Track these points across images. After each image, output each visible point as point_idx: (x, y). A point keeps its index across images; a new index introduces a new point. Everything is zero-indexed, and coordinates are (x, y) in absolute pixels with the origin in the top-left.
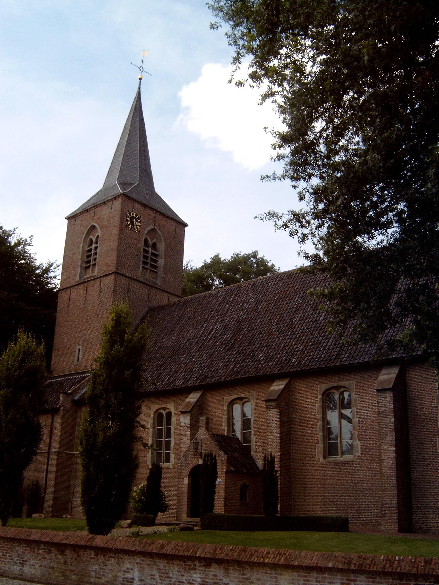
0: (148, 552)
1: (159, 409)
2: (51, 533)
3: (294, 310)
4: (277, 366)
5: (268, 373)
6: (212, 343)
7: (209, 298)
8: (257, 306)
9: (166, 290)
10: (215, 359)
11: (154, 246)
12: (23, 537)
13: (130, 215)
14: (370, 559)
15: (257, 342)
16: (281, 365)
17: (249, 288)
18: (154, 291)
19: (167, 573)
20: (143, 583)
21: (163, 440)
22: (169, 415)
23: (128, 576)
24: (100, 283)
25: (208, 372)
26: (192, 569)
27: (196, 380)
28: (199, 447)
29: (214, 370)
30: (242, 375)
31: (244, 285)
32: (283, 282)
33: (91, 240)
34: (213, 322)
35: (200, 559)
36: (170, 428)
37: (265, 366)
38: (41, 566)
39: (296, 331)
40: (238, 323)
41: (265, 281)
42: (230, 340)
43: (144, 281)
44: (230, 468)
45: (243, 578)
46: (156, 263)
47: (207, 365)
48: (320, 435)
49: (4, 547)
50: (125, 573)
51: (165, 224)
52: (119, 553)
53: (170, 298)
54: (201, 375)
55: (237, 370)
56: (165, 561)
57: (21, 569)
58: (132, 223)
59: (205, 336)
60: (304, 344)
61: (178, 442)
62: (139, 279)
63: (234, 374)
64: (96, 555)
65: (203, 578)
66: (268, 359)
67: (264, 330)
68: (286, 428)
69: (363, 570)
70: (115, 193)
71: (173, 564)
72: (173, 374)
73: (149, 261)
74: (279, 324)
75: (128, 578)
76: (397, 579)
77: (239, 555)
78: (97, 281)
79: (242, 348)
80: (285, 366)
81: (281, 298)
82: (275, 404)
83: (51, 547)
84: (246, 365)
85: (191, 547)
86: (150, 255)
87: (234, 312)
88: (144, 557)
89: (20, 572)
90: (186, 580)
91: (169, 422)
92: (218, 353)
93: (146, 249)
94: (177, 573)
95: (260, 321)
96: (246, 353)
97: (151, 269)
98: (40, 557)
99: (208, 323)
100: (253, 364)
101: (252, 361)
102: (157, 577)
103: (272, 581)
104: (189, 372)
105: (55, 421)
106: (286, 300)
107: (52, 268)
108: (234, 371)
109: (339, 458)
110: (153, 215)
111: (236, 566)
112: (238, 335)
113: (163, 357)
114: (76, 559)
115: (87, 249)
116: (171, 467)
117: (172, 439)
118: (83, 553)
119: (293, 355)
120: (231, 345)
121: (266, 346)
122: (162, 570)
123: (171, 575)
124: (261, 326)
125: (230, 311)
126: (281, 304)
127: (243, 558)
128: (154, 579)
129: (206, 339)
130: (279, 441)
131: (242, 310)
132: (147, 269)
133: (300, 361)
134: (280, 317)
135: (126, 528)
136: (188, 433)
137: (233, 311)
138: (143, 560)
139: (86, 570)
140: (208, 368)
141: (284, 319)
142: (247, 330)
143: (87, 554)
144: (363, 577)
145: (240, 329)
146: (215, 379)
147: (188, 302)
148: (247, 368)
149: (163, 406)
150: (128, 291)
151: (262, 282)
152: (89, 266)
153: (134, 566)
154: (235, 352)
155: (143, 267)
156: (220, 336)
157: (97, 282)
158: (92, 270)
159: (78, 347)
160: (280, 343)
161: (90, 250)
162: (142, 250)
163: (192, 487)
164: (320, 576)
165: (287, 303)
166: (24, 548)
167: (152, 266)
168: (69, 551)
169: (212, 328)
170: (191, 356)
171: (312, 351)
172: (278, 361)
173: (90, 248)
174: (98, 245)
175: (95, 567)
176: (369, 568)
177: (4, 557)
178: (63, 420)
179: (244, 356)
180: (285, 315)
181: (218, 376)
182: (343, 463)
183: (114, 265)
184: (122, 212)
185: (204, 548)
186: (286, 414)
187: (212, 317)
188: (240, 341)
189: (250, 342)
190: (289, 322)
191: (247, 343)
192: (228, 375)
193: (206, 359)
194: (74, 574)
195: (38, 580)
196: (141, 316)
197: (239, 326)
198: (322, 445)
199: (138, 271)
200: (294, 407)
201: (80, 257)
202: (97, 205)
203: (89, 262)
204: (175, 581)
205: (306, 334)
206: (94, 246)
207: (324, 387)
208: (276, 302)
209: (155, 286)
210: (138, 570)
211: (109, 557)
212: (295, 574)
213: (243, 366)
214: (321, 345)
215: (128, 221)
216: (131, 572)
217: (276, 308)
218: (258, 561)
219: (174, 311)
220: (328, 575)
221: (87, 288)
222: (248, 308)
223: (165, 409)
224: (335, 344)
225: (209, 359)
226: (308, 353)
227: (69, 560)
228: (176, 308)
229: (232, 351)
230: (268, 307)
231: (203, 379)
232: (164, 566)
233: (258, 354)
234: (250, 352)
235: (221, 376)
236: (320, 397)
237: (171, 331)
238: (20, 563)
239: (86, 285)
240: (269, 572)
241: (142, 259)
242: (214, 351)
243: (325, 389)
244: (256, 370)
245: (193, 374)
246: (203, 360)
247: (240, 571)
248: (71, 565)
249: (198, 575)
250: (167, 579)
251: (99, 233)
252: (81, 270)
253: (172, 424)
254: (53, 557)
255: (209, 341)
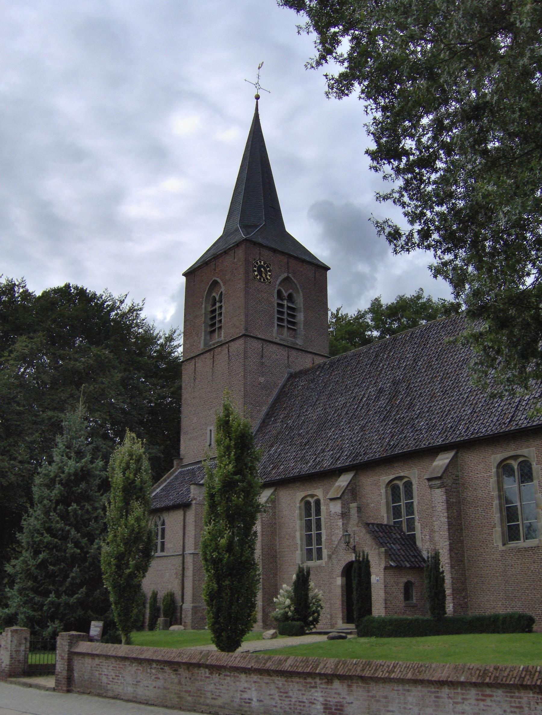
0: (264, 669)
1: (306, 497)
2: (152, 649)
3: (460, 364)
4: (440, 436)
5: (431, 445)
6: (364, 412)
7: (360, 356)
8: (417, 363)
9: (310, 350)
10: (369, 432)
11: (290, 298)
12: (134, 656)
13: (257, 263)
14: (508, 670)
15: (417, 407)
16: (445, 435)
17: (406, 340)
18: (294, 353)
19: (286, 693)
20: (261, 703)
21: (313, 533)
22: (318, 502)
23: (245, 696)
24: (229, 350)
25: (360, 448)
26: (313, 687)
27: (347, 459)
28: (352, 540)
29: (367, 446)
30: (399, 450)
31: (400, 337)
32: (447, 330)
33: (214, 298)
34: (365, 386)
35: (320, 674)
36: (320, 519)
37: (427, 436)
38: (155, 687)
39: (463, 390)
40: (394, 385)
41: (425, 330)
42: (385, 406)
43: (282, 342)
44: (389, 563)
45: (368, 696)
46: (294, 319)
47: (359, 440)
48: (496, 517)
49: (116, 667)
50: (242, 693)
51: (301, 269)
52: (235, 671)
53: (315, 359)
54: (351, 453)
55: (394, 444)
56: (284, 679)
57: (135, 691)
58: (260, 273)
59: (356, 404)
60: (473, 406)
61: (330, 535)
62: (274, 340)
63: (391, 448)
64: (211, 673)
65: (326, 696)
66: (432, 427)
67: (425, 392)
68: (455, 511)
69: (499, 683)
70: (236, 239)
71: (292, 682)
72: (319, 453)
73: (285, 317)
74: (443, 383)
75: (245, 699)
76: (538, 693)
77: (363, 670)
78: (225, 347)
79: (399, 416)
80: (451, 435)
81: (445, 350)
82: (439, 482)
83: (164, 666)
84: (405, 437)
85: (310, 663)
86: (285, 310)
87: (389, 372)
88: (261, 674)
89: (133, 694)
90: (307, 699)
91: (318, 512)
92: (371, 424)
93: (281, 302)
94: (297, 692)
95: (420, 381)
96: (404, 421)
97: (289, 326)
98: (153, 677)
99: (359, 388)
100: (413, 435)
101: (412, 432)
102: (277, 697)
103: (399, 698)
104: (338, 449)
105: (187, 518)
106: (450, 352)
107: (175, 335)
108: (390, 445)
109: (522, 544)
110: (286, 260)
111: (360, 683)
112: (395, 400)
113: (307, 433)
114: (190, 678)
115: (210, 309)
116: (324, 565)
117: (323, 532)
118: (197, 671)
119: (459, 421)
120: (387, 413)
121: (428, 412)
122: (281, 688)
123: (290, 694)
124: (422, 387)
125: (384, 370)
126: (444, 358)
127: (367, 673)
128: (273, 699)
129: (357, 407)
130: (447, 527)
131: (399, 368)
132: (283, 326)
133: (468, 427)
134: (444, 374)
135: (268, 639)
136: (340, 523)
137: (388, 370)
138: (260, 679)
139: (201, 690)
140: (360, 444)
141: (448, 376)
142: (405, 394)
143: (201, 673)
144: (500, 692)
145: (397, 392)
146: (368, 456)
147: (334, 363)
148: (406, 441)
149: (310, 493)
150: (262, 356)
151: (421, 331)
152: (214, 331)
153: (251, 685)
154: (391, 422)
155: (278, 325)
156: (373, 402)
157: (225, 349)
158: (218, 335)
159: (209, 428)
160: (444, 407)
161: (214, 311)
162: (276, 305)
163: (348, 589)
164: (452, 691)
165: (452, 356)
166: (136, 668)
167: (289, 322)
168: (182, 670)
169: (364, 394)
170: (340, 430)
171: (482, 414)
172: (443, 429)
173: (214, 308)
174: (223, 303)
175: (211, 687)
176: (506, 681)
177: (117, 678)
178: (196, 515)
179: (402, 425)
180: (450, 371)
181: (371, 453)
182: (526, 549)
183: (242, 327)
184: (247, 261)
185: (325, 662)
186: (454, 494)
187: (363, 379)
188: (397, 407)
189: (409, 408)
190: (455, 379)
191: (405, 409)
192: (383, 451)
193: (357, 433)
194: (189, 696)
195: (153, 703)
196: (280, 385)
197: (396, 388)
198: (500, 529)
199: (272, 330)
200: (463, 484)
201: (203, 319)
202: (218, 255)
203: (213, 325)
204: (296, 701)
205: (475, 393)
206: (218, 305)
207: (499, 457)
208: (438, 355)
209: (294, 346)
210: (256, 690)
211: (225, 675)
212: (425, 690)
213: (401, 438)
214: (493, 405)
215: (255, 271)
216: (249, 691)
217: (438, 364)
218: (383, 676)
219: (319, 376)
220: (462, 689)
221: (213, 357)
222: (406, 365)
223: (312, 496)
224: (510, 404)
225: (361, 431)
226: (477, 416)
227: (183, 681)
228: (321, 372)
229: (388, 421)
230: (429, 363)
231: (354, 457)
232: (283, 684)
233: (418, 422)
234: (408, 420)
235: (375, 452)
236: (494, 470)
237: (317, 401)
238: (133, 684)
239: (212, 353)
240: (396, 688)
241: (276, 316)
242: (367, 422)
243: (500, 460)
244: (416, 443)
245: (342, 452)
246: (354, 434)
247: (364, 687)
248: (186, 685)
249: (320, 694)
250: (287, 699)
251: (223, 289)
252: (205, 335)
253: (322, 513)
254: (167, 676)
255: (361, 410)
